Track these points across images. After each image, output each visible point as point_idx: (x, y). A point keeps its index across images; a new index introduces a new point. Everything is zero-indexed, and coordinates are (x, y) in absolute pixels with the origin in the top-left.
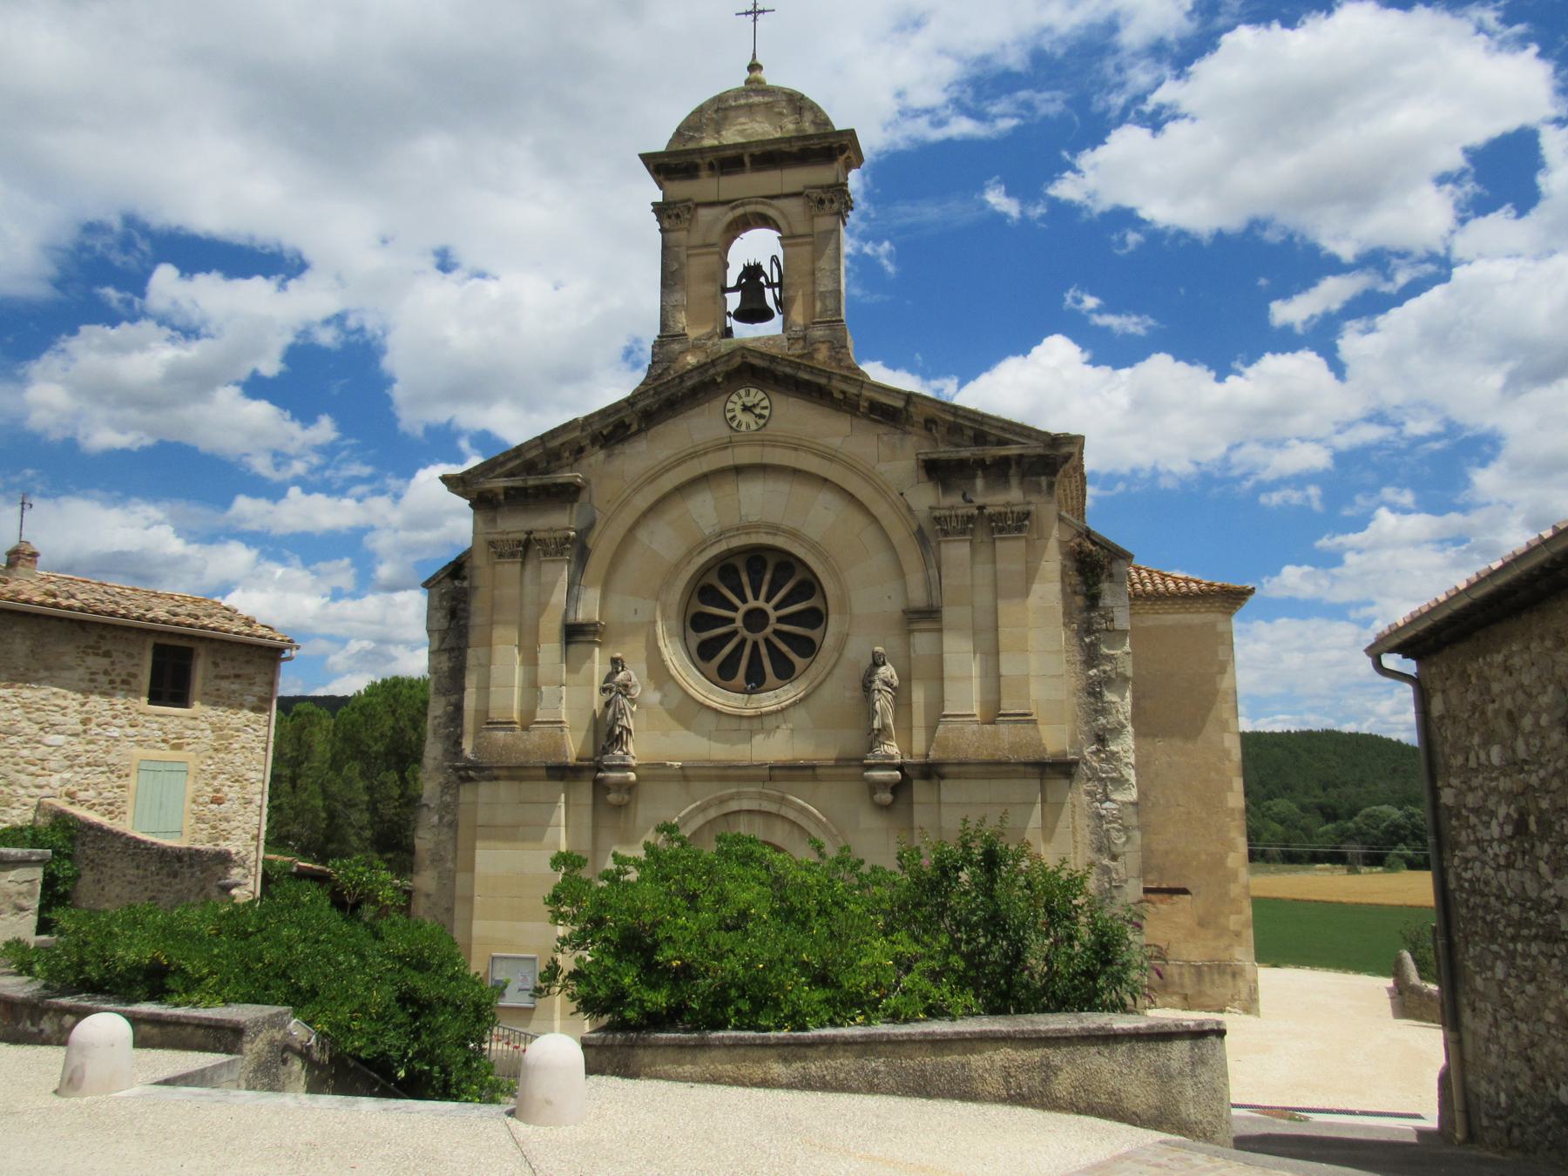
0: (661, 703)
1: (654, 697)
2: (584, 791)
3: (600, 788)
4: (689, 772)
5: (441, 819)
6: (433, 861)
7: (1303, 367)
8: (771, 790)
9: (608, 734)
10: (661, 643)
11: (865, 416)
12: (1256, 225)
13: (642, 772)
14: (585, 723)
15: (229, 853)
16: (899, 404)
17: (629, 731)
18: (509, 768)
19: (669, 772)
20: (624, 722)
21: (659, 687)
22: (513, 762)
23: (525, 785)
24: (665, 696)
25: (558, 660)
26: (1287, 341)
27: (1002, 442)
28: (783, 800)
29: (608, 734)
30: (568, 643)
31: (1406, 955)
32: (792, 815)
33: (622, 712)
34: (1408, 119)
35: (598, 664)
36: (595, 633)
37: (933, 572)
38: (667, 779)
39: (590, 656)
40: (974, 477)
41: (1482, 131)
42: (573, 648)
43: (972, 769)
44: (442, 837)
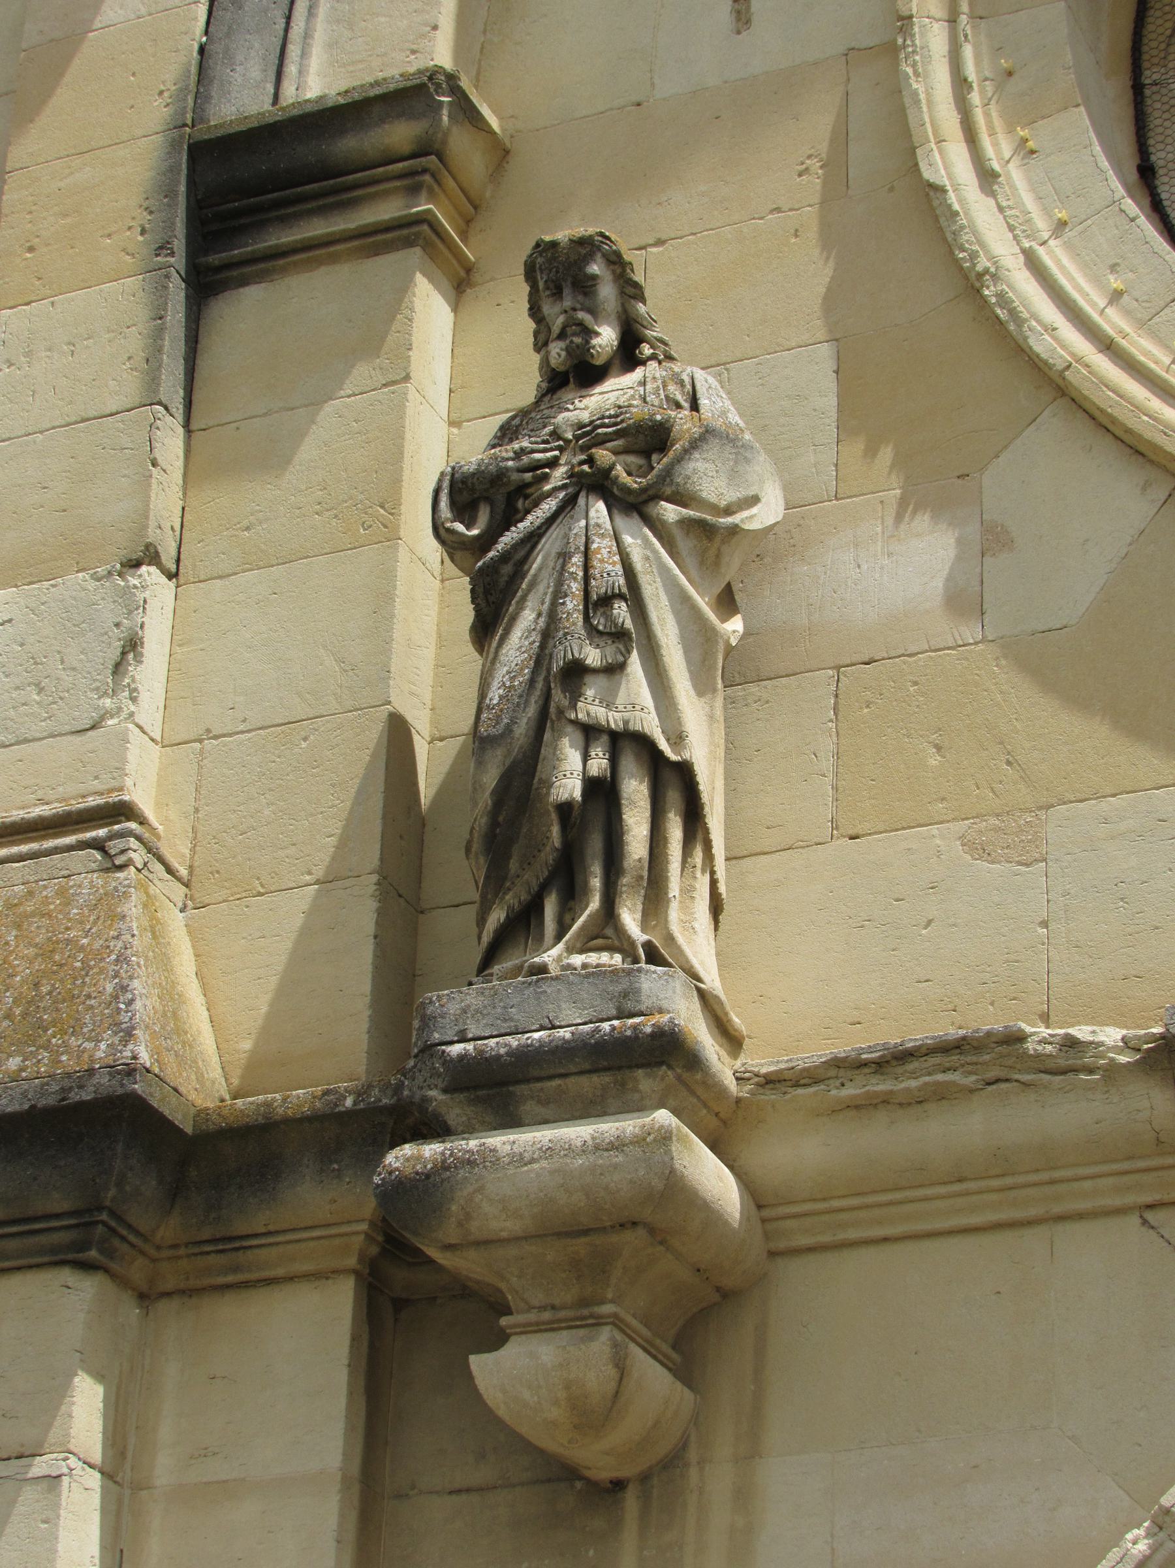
0: (965, 601)
1: (891, 569)
2: (294, 1347)
3: (417, 1304)
9: (524, 838)
10: (949, 164)
13: (800, 1151)
14: (318, 816)
15: (737, 526)
17: (674, 782)
19: (1065, 1116)
20: (632, 702)
21: (936, 481)
24: (994, 540)
25: (124, 386)
29: (524, 838)
30: (206, 283)
33: (614, 612)
35: (444, 373)
36: (423, 164)
38: (1023, 1198)
39: (377, 336)
42: (245, 312)
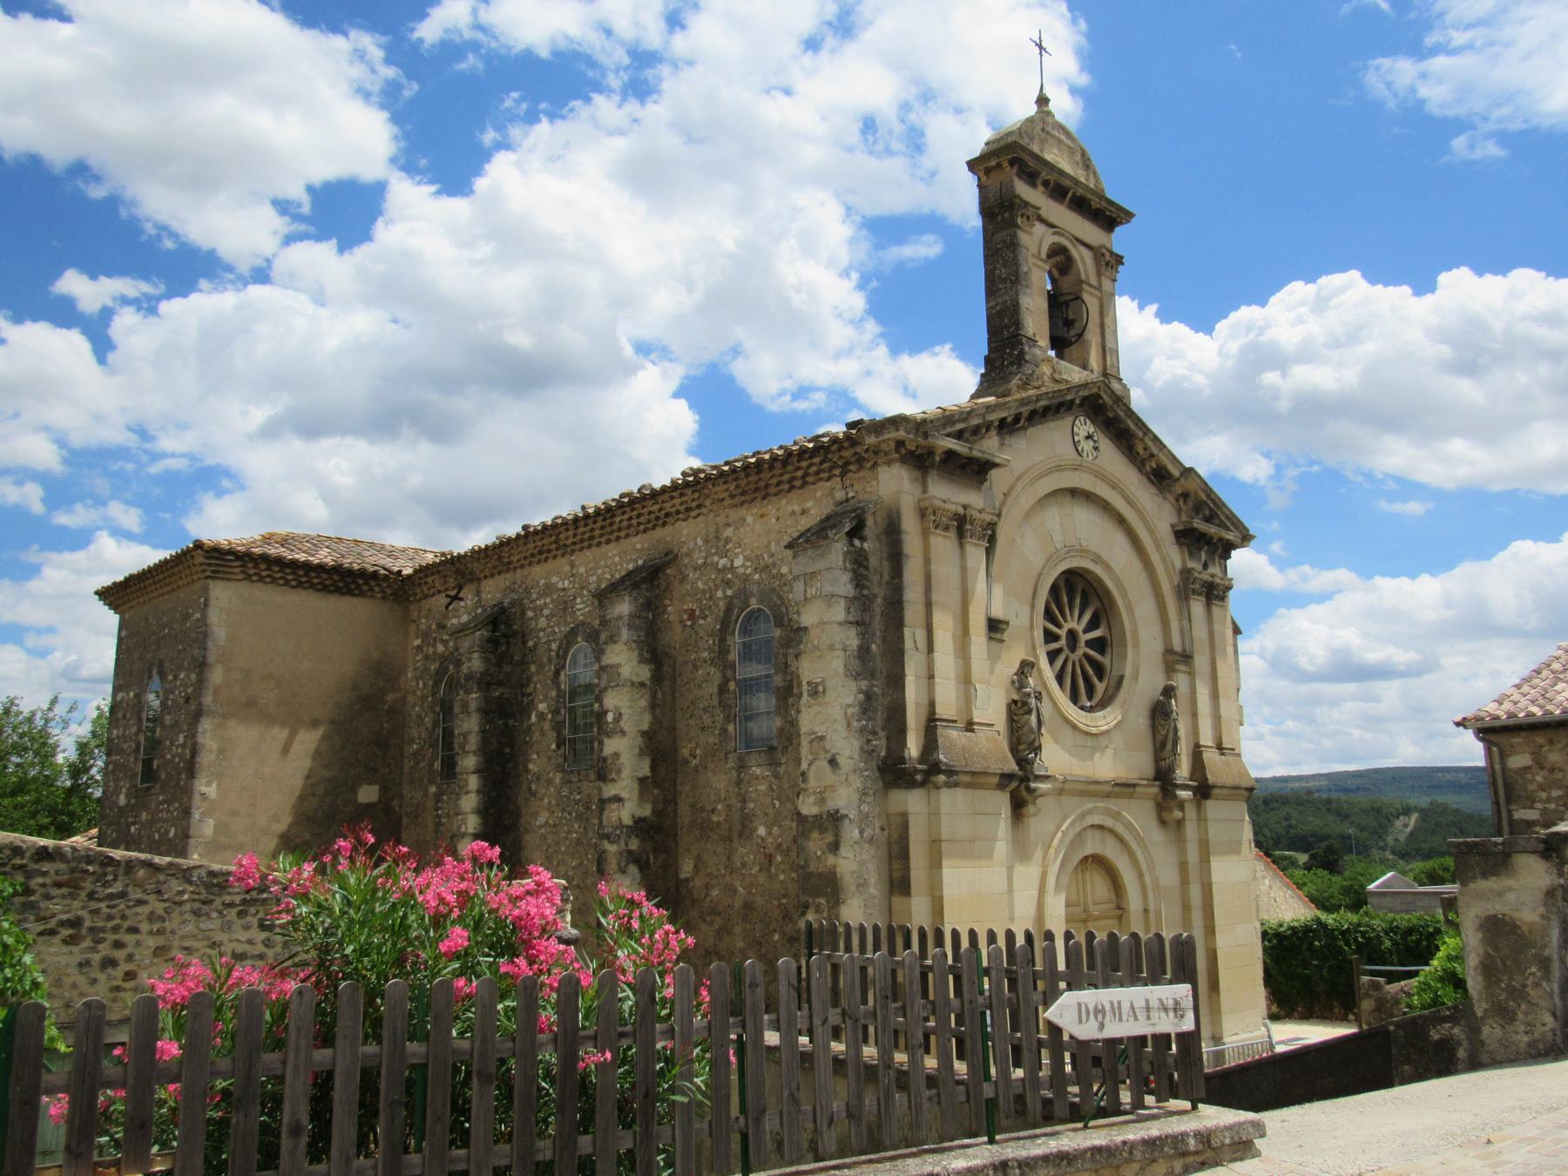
4: (1067, 786)
5: (862, 832)
6: (859, 886)
7: (69, 346)
8: (1113, 805)
11: (1147, 475)
12: (80, 169)
16: (1176, 473)
18: (973, 773)
22: (978, 768)
23: (978, 793)
26: (64, 314)
27: (1222, 525)
28: (1117, 816)
31: (951, 977)
32: (1120, 829)
34: (261, 123)
37: (1186, 622)
40: (1200, 549)
41: (325, 170)
43: (1225, 792)
44: (865, 857)
